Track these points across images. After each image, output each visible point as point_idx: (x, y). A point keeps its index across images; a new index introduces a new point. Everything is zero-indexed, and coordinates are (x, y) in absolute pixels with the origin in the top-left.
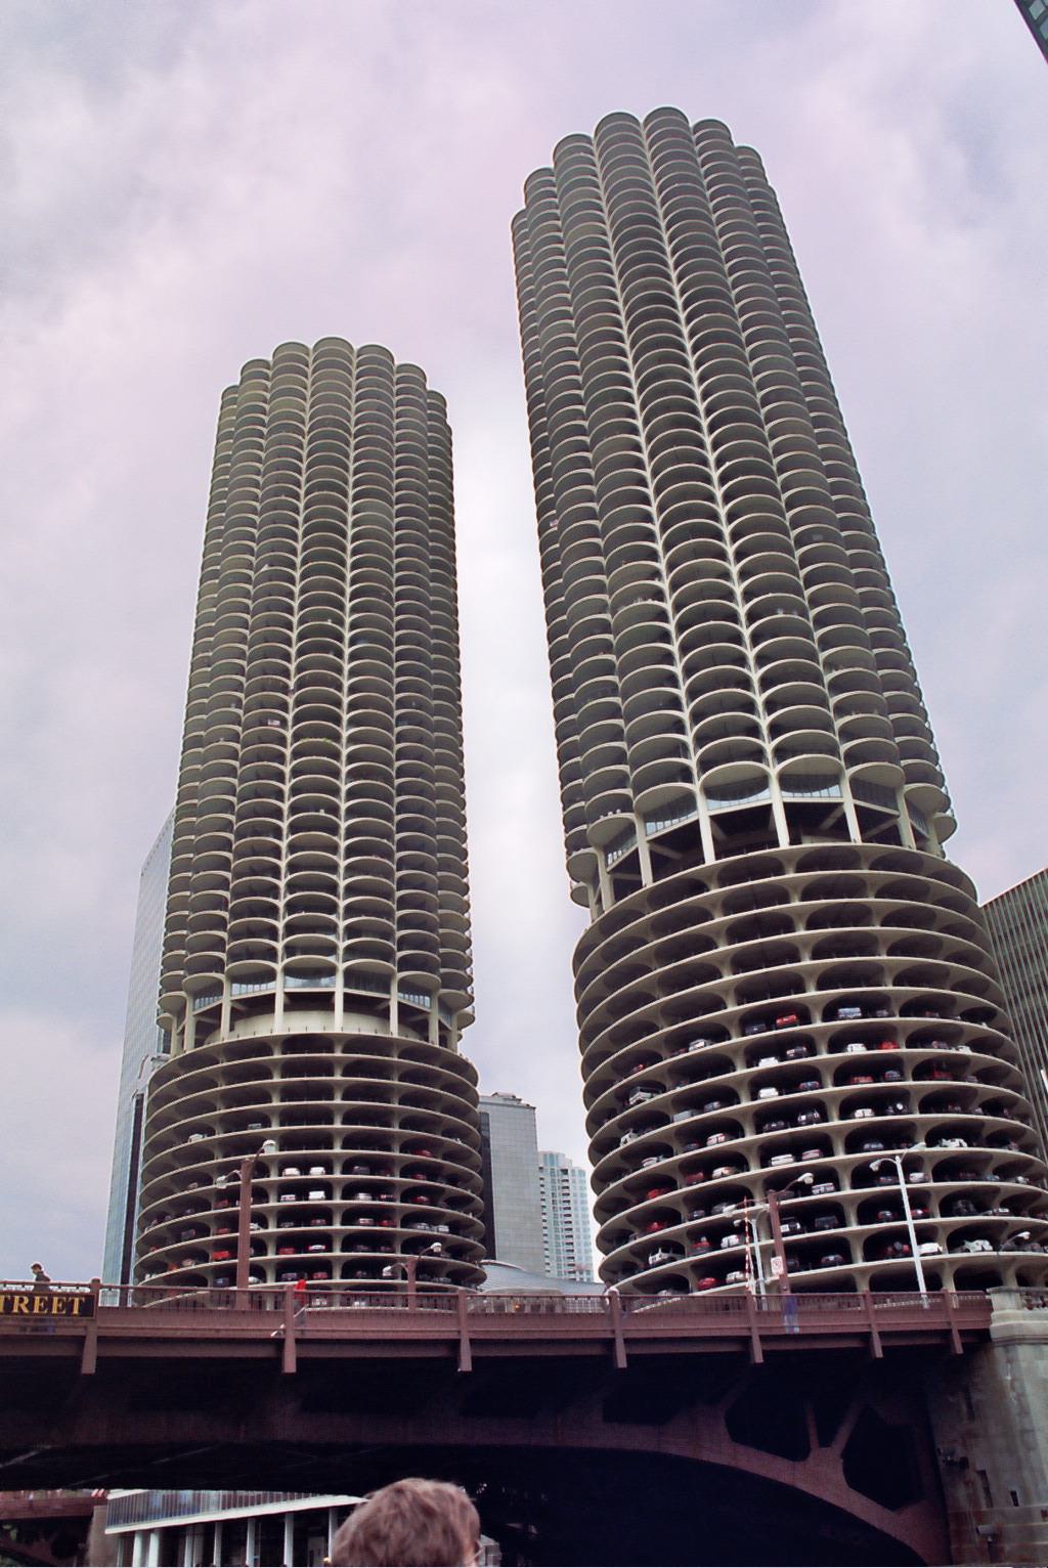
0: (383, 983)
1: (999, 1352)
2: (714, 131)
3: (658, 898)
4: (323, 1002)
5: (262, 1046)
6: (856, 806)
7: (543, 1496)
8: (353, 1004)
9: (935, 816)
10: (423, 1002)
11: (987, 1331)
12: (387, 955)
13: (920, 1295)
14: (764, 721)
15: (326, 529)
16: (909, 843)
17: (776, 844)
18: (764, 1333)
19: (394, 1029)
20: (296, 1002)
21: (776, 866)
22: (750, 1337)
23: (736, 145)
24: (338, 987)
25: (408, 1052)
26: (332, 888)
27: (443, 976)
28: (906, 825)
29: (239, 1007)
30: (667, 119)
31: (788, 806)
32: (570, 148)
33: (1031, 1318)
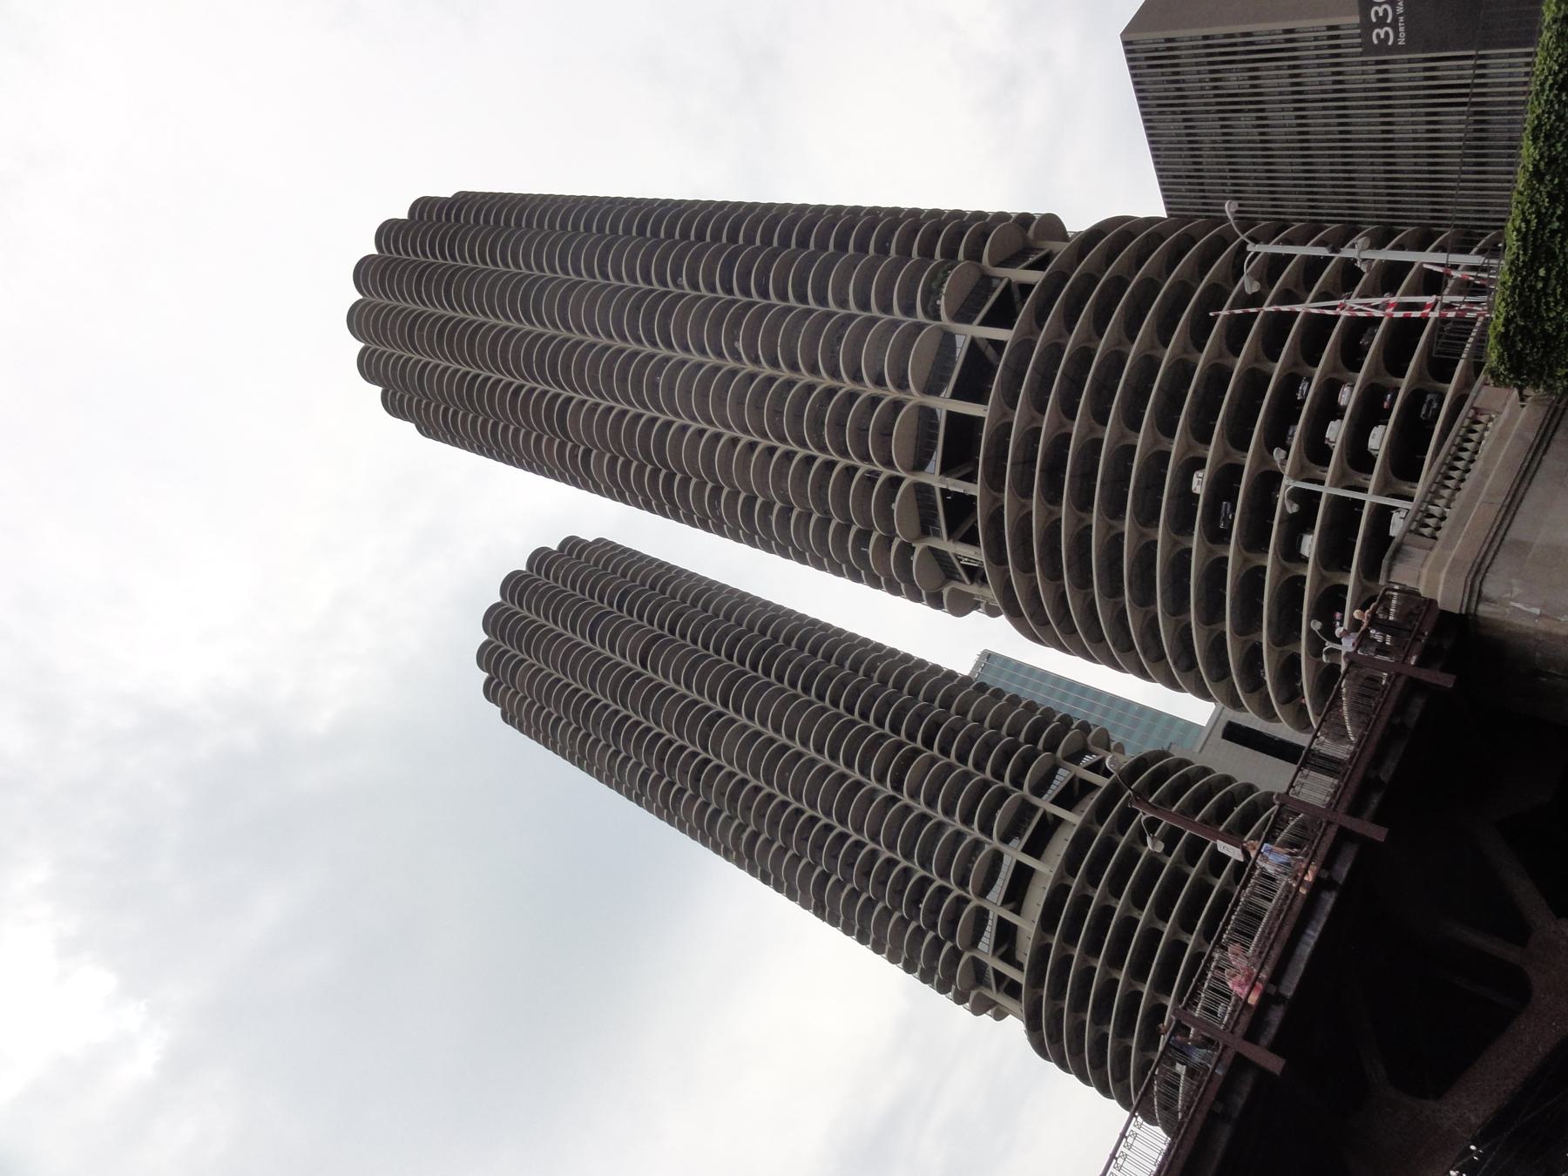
0: (1026, 809)
1: (1484, 610)
2: (388, 233)
3: (997, 557)
4: (1023, 876)
5: (1041, 952)
8: (1036, 847)
9: (1028, 235)
10: (1062, 777)
11: (1445, 614)
12: (1004, 794)
13: (1309, 749)
15: (624, 684)
16: (1036, 277)
17: (981, 419)
19: (1074, 819)
20: (1015, 897)
23: (405, 216)
24: (1013, 854)
26: (924, 818)
28: (1020, 275)
29: (1002, 950)
30: (364, 273)
31: (956, 395)
32: (369, 367)
33: (1449, 545)
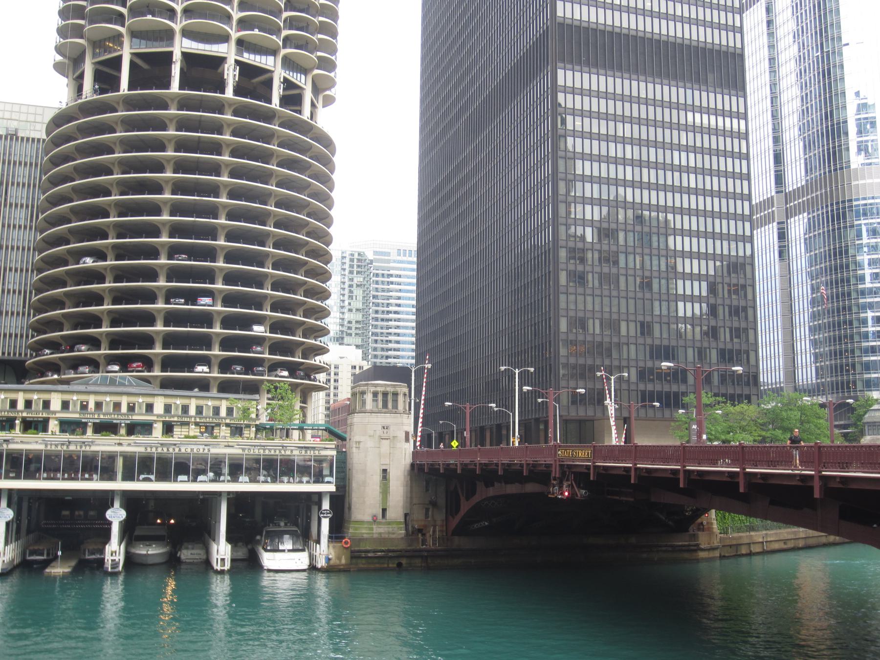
3: (130, 103)
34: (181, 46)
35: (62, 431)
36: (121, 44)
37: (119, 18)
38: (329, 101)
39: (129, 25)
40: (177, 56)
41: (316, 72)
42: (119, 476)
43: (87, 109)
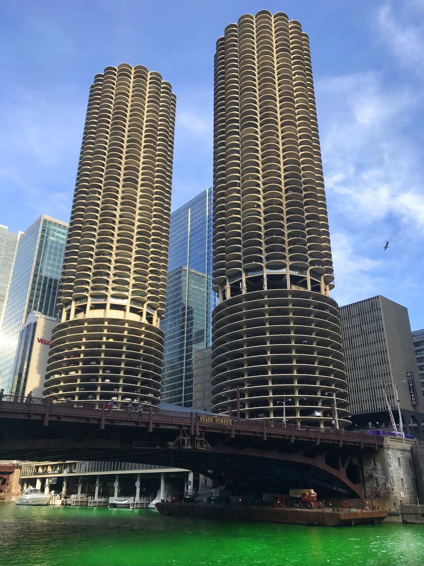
3: (247, 298)
4: (122, 308)
6: (311, 279)
7: (209, 471)
14: (287, 248)
18: (200, 425)
19: (144, 320)
21: (286, 294)
22: (149, 423)
25: (148, 327)
27: (160, 304)
29: (93, 306)
34: (266, 272)
35: (21, 466)
36: (241, 276)
37: (239, 265)
38: (332, 287)
39: (243, 236)
40: (265, 277)
41: (325, 275)
42: (38, 309)
43: (230, 302)
